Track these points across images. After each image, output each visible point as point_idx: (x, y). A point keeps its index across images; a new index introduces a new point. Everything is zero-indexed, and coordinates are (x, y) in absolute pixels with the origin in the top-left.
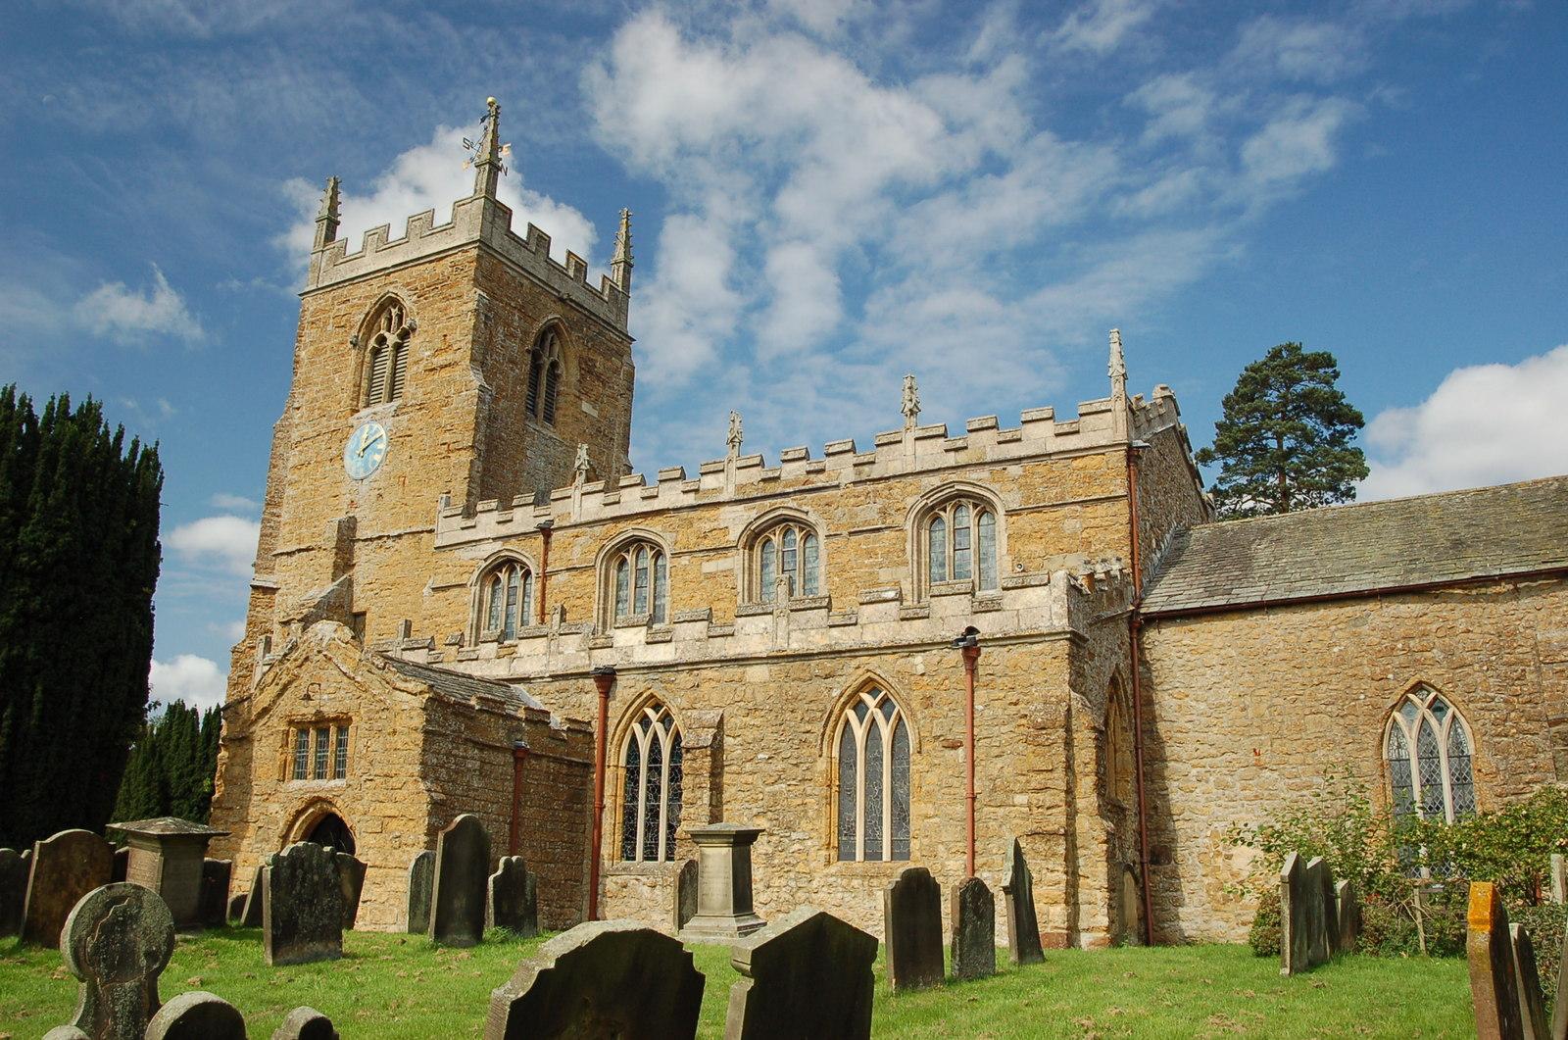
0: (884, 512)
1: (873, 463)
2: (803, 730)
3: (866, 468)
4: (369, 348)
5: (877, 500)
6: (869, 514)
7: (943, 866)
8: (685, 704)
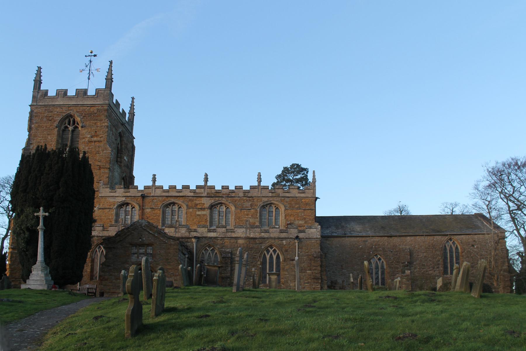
0: (251, 205)
1: (249, 192)
3: (247, 194)
4: (61, 129)
7: (289, 285)
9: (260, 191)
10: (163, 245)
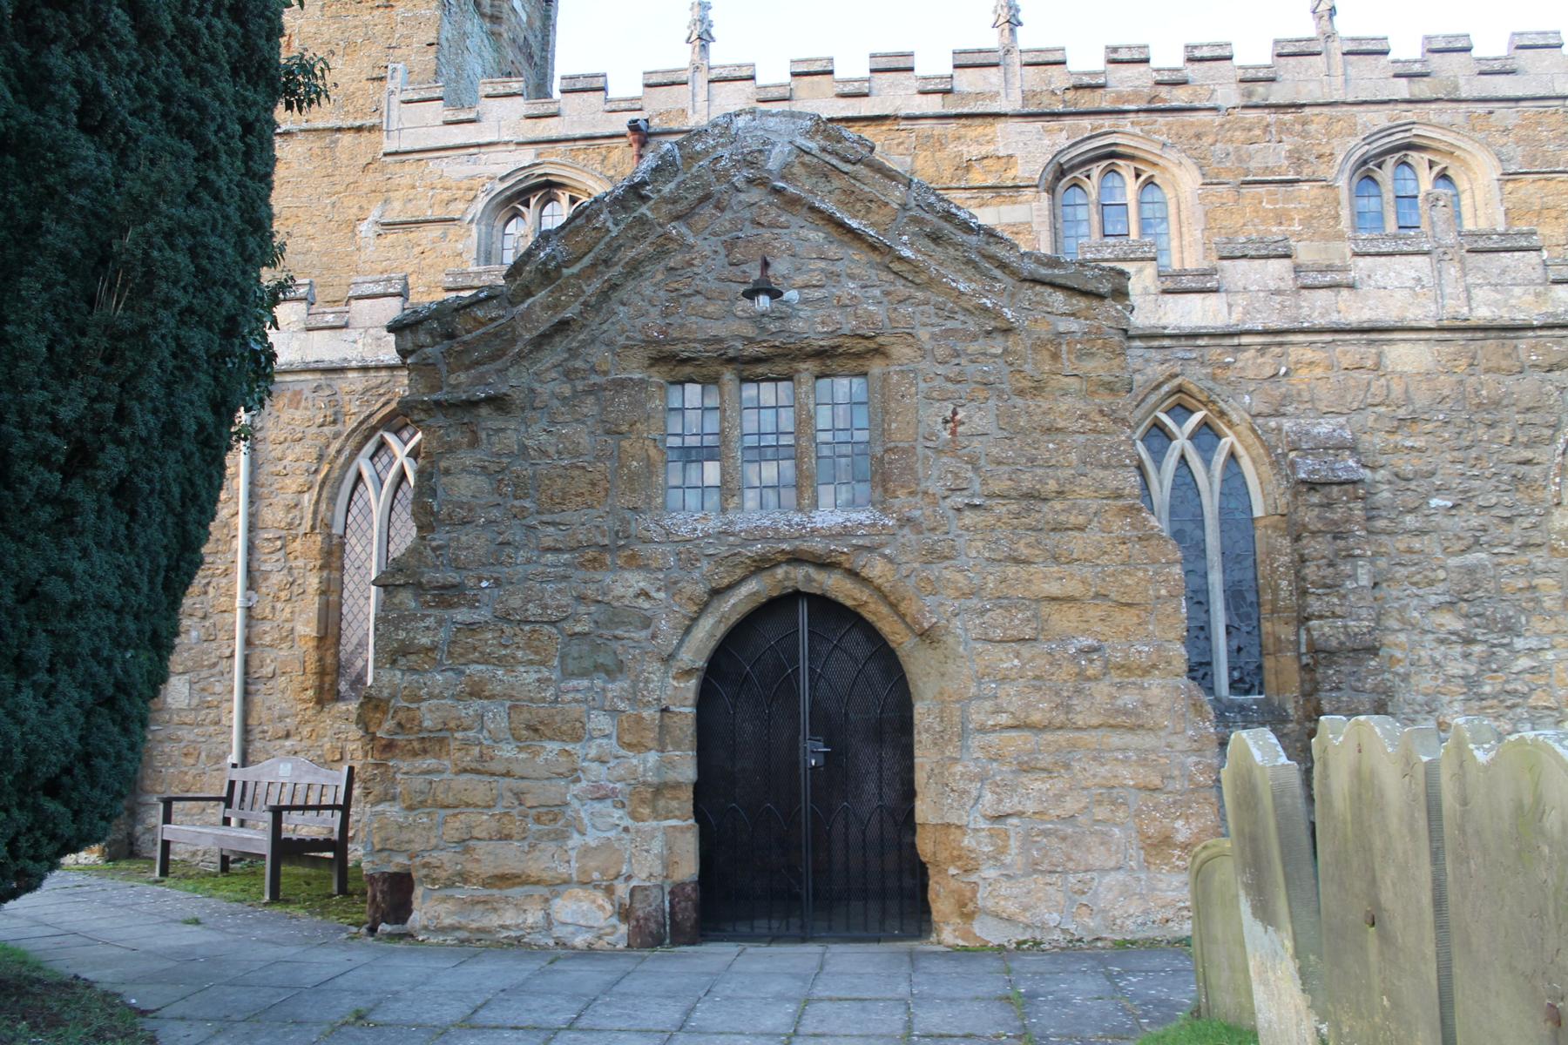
0: (1297, 158)
1: (1273, 80)
2: (1516, 457)
3: (1260, 88)
5: (1284, 138)
6: (1273, 156)
8: (1259, 406)
9: (1340, 71)
10: (973, 348)
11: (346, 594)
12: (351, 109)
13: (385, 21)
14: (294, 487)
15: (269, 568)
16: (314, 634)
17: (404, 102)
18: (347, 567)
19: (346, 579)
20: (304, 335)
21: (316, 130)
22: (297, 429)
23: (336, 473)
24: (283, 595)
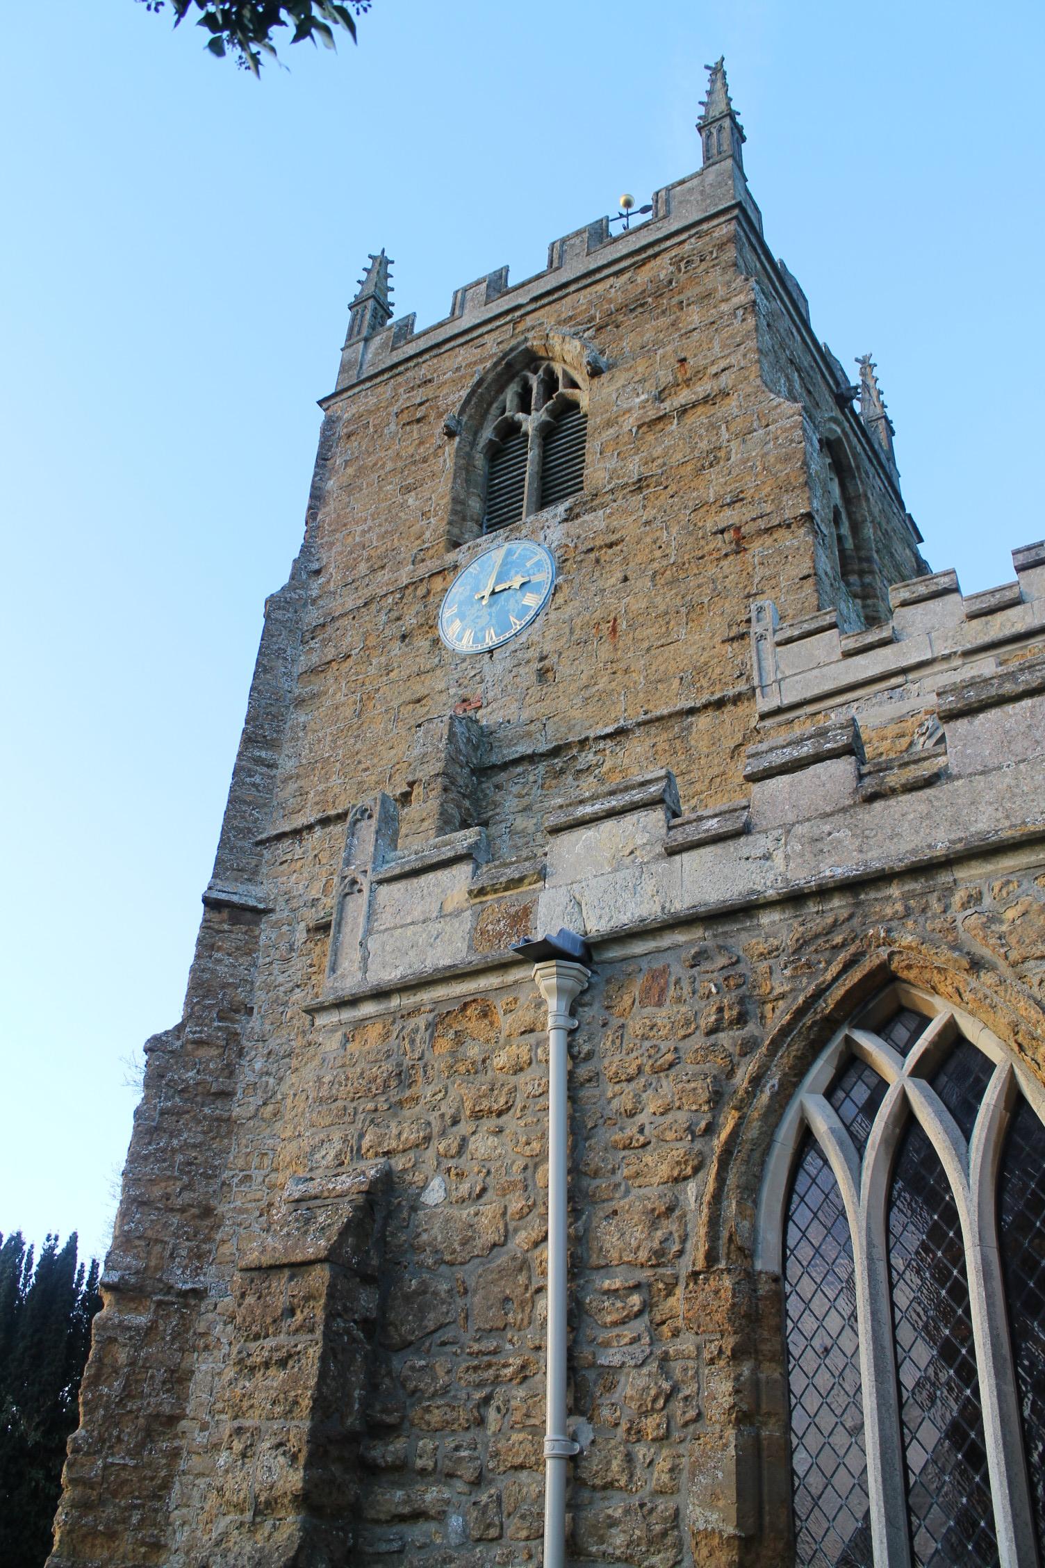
11: (799, 1421)
12: (704, 683)
13: (738, 568)
14: (664, 1170)
15: (616, 1360)
16: (730, 1530)
17: (779, 644)
18: (796, 1352)
19: (797, 1382)
20: (664, 864)
21: (659, 719)
22: (664, 1046)
23: (752, 1131)
24: (651, 1425)
